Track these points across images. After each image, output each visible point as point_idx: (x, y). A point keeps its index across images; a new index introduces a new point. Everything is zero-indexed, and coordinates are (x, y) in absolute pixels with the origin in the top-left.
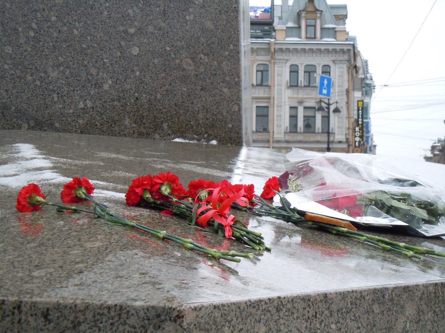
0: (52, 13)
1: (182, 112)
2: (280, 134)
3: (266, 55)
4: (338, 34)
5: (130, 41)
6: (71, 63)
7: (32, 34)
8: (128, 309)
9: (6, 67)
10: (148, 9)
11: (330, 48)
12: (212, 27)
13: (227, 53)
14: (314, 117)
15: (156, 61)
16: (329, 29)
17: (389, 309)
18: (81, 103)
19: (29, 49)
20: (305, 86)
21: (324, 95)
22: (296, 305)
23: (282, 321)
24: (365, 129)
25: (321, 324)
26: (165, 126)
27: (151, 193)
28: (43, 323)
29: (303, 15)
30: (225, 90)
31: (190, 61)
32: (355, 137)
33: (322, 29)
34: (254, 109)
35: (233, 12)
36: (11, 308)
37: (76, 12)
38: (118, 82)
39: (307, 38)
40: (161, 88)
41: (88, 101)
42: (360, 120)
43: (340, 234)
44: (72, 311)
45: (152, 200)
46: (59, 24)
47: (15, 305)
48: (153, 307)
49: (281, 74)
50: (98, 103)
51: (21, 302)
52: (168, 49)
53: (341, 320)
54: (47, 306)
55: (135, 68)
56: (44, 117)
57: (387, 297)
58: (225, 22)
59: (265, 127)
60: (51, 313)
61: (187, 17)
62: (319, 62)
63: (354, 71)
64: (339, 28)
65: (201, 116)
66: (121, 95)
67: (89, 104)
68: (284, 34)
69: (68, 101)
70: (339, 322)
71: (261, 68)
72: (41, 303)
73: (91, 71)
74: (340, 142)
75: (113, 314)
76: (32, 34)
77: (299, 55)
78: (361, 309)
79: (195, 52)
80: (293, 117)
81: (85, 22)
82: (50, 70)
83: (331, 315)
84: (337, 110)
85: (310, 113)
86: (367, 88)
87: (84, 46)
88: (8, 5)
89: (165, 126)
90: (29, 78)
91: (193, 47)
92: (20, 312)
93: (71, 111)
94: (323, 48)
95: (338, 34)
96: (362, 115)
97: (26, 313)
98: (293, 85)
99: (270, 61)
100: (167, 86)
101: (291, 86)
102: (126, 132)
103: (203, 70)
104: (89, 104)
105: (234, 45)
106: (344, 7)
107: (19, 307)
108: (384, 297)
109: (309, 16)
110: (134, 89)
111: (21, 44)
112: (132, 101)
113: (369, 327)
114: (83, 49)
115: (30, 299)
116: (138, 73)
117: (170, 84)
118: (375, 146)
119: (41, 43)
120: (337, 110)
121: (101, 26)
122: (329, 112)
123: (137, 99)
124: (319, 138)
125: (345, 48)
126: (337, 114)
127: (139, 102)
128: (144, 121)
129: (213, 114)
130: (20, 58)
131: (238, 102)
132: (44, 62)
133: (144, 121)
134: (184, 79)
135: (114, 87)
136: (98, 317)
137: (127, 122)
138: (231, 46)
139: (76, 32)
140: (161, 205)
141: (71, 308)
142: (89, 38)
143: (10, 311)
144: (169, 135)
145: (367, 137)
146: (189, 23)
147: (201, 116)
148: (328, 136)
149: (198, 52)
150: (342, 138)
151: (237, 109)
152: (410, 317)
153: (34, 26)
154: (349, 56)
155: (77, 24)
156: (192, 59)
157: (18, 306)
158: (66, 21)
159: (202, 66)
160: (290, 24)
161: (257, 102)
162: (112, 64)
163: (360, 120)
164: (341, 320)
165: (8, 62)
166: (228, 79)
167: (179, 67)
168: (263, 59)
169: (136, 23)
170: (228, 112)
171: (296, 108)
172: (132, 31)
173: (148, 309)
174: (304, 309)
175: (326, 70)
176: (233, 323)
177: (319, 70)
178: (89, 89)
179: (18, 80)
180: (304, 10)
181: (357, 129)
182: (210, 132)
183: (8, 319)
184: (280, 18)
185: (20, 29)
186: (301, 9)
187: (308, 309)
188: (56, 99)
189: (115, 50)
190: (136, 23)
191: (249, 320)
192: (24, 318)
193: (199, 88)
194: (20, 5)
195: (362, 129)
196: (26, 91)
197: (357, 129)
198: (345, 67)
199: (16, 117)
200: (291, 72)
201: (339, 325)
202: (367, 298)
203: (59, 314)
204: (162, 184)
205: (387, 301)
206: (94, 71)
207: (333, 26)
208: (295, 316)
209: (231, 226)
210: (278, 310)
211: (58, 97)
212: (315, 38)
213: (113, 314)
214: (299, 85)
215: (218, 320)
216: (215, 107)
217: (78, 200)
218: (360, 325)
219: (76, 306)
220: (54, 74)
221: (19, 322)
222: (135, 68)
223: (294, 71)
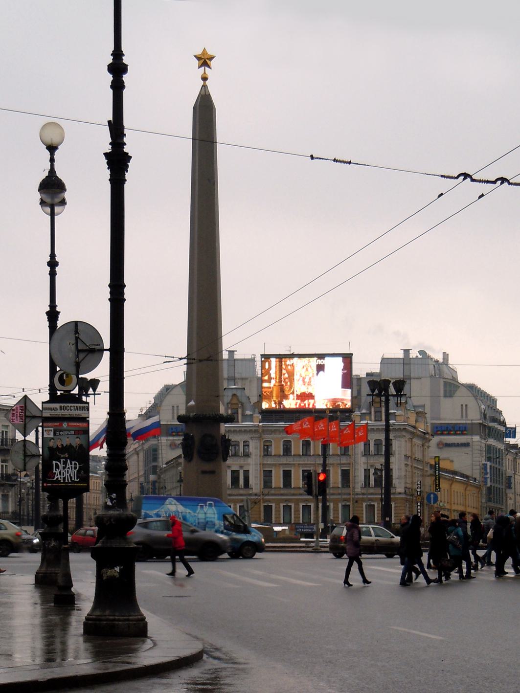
4: (397, 417)
39: (375, 420)
74: (400, 493)
77: (381, 433)
80: (367, 477)
98: (367, 453)
150: (402, 490)
160: (364, 411)
175: (246, 444)
200: (374, 444)
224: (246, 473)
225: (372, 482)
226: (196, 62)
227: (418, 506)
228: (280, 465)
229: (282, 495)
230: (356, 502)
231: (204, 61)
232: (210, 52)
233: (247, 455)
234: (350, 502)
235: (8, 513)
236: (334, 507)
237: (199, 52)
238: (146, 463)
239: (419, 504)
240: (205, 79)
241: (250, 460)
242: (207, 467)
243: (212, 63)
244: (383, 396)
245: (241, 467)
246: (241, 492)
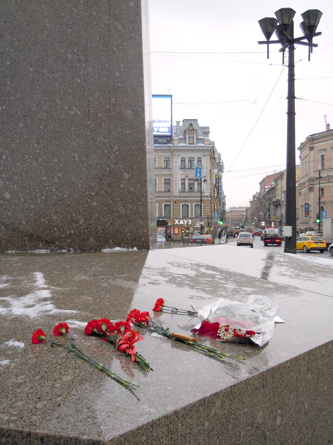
0: (53, 187)
1: (119, 233)
2: (177, 193)
3: (169, 153)
4: (205, 141)
5: (92, 199)
6: (63, 212)
7: (44, 198)
8: (80, 440)
9: (31, 215)
10: (101, 182)
11: (201, 148)
12: (133, 190)
13: (141, 203)
14: (194, 184)
15: (106, 208)
16: (200, 139)
17: (208, 407)
18: (69, 231)
19: (42, 206)
20: (189, 168)
21: (198, 176)
22: (161, 421)
23: (154, 431)
24: (219, 189)
25: (174, 425)
26: (111, 241)
27: (97, 329)
28: (41, 443)
29: (187, 132)
30: (141, 222)
31: (123, 208)
32: (215, 193)
33: (197, 139)
34: (163, 180)
35: (144, 182)
36: (26, 434)
37: (65, 185)
38: (87, 220)
40: (108, 222)
41: (72, 230)
42: (217, 184)
43: (189, 344)
44: (54, 438)
45: (97, 332)
46: (57, 192)
47: (27, 433)
48: (91, 440)
49: (176, 162)
50: (77, 231)
51: (30, 432)
52: (112, 202)
53: (183, 420)
54: (42, 435)
55: (95, 213)
56: (50, 240)
57: (206, 401)
58: (140, 187)
59: (169, 189)
60: (44, 438)
61: (121, 186)
62: (196, 156)
63: (214, 160)
64: (206, 138)
65: (128, 235)
66: (88, 226)
67: (72, 232)
68: (177, 141)
69: (62, 230)
70: (182, 422)
71: (166, 159)
72: (39, 433)
73: (73, 215)
74: (207, 197)
75: (73, 441)
76: (44, 198)
78: (194, 411)
79: (125, 203)
80: (183, 184)
81: (70, 191)
82: (53, 215)
83: (179, 419)
84: (205, 181)
85: (192, 182)
86: (220, 168)
87: (69, 202)
88: (32, 184)
89: (111, 241)
90: (43, 220)
91: (124, 201)
92: (30, 437)
93: (64, 236)
94: (197, 148)
95: (205, 142)
96: (218, 182)
97: (33, 438)
98: (183, 168)
99: (171, 156)
100: (111, 221)
101: (181, 168)
102: (91, 245)
103: (129, 212)
104: (72, 232)
105: (144, 199)
106: (208, 128)
107: (30, 435)
108: (205, 402)
109: (190, 132)
110: (95, 223)
111: (38, 203)
112: (94, 229)
113: (198, 418)
114: (69, 204)
115: (34, 431)
116: (96, 215)
117: (113, 220)
118: (225, 196)
119: (48, 202)
120: (205, 181)
121: (78, 192)
122: (201, 182)
123: (96, 228)
124: (196, 195)
125: (209, 149)
126: (205, 182)
127: (97, 230)
128: (100, 239)
129: (134, 234)
130: (38, 210)
131: (147, 227)
132: (50, 212)
133: (100, 239)
134: (120, 217)
135: (85, 223)
136: (66, 442)
137: (91, 240)
138: (143, 199)
139: (65, 196)
140: (102, 336)
141: (53, 437)
142: (72, 198)
143: (25, 436)
144: (113, 245)
145: (221, 193)
146: (121, 188)
147: (128, 235)
148: (201, 194)
149: (126, 203)
150: (208, 194)
151: (146, 231)
152: (218, 407)
153: (45, 194)
154: (211, 152)
155: (66, 192)
156: (124, 206)
157: (29, 434)
158: (60, 190)
159: (128, 210)
160: (181, 137)
161: (164, 177)
162: (83, 211)
163: (217, 184)
164: (183, 420)
165: (33, 212)
166: (142, 216)
167: (117, 211)
168: (167, 154)
169: (95, 190)
170: (142, 233)
171: (185, 179)
172: (93, 194)
173: (89, 441)
174: (165, 421)
175: (199, 161)
176: (130, 440)
177: (196, 160)
178: (72, 224)
179: (37, 221)
180: (187, 130)
181: (216, 190)
182: (133, 243)
183: (24, 440)
184: (176, 134)
185: (38, 196)
186: (187, 129)
187: (167, 421)
188: (56, 230)
189: (85, 204)
190: (95, 190)
191: (138, 436)
192: (32, 440)
193: (127, 221)
194: (38, 184)
195: (218, 189)
196: (41, 227)
197: (216, 190)
198: (209, 158)
199: (37, 240)
201: (182, 423)
202: (196, 405)
203: (48, 440)
204: (102, 324)
205: (206, 403)
206: (74, 215)
207: (203, 137)
208: (161, 426)
209: (134, 355)
210: (152, 426)
211: (57, 229)
212: (193, 143)
213: (73, 441)
214: (186, 168)
215: (122, 441)
216: (135, 230)
217: (61, 334)
218: (193, 419)
219: (56, 436)
220: (55, 218)
221: (30, 441)
222: (95, 213)
223: (183, 161)
225: (187, 187)
227: (215, 206)
228: (162, 175)
230: (176, 202)
234: (171, 202)
236: (159, 206)
239: (216, 204)
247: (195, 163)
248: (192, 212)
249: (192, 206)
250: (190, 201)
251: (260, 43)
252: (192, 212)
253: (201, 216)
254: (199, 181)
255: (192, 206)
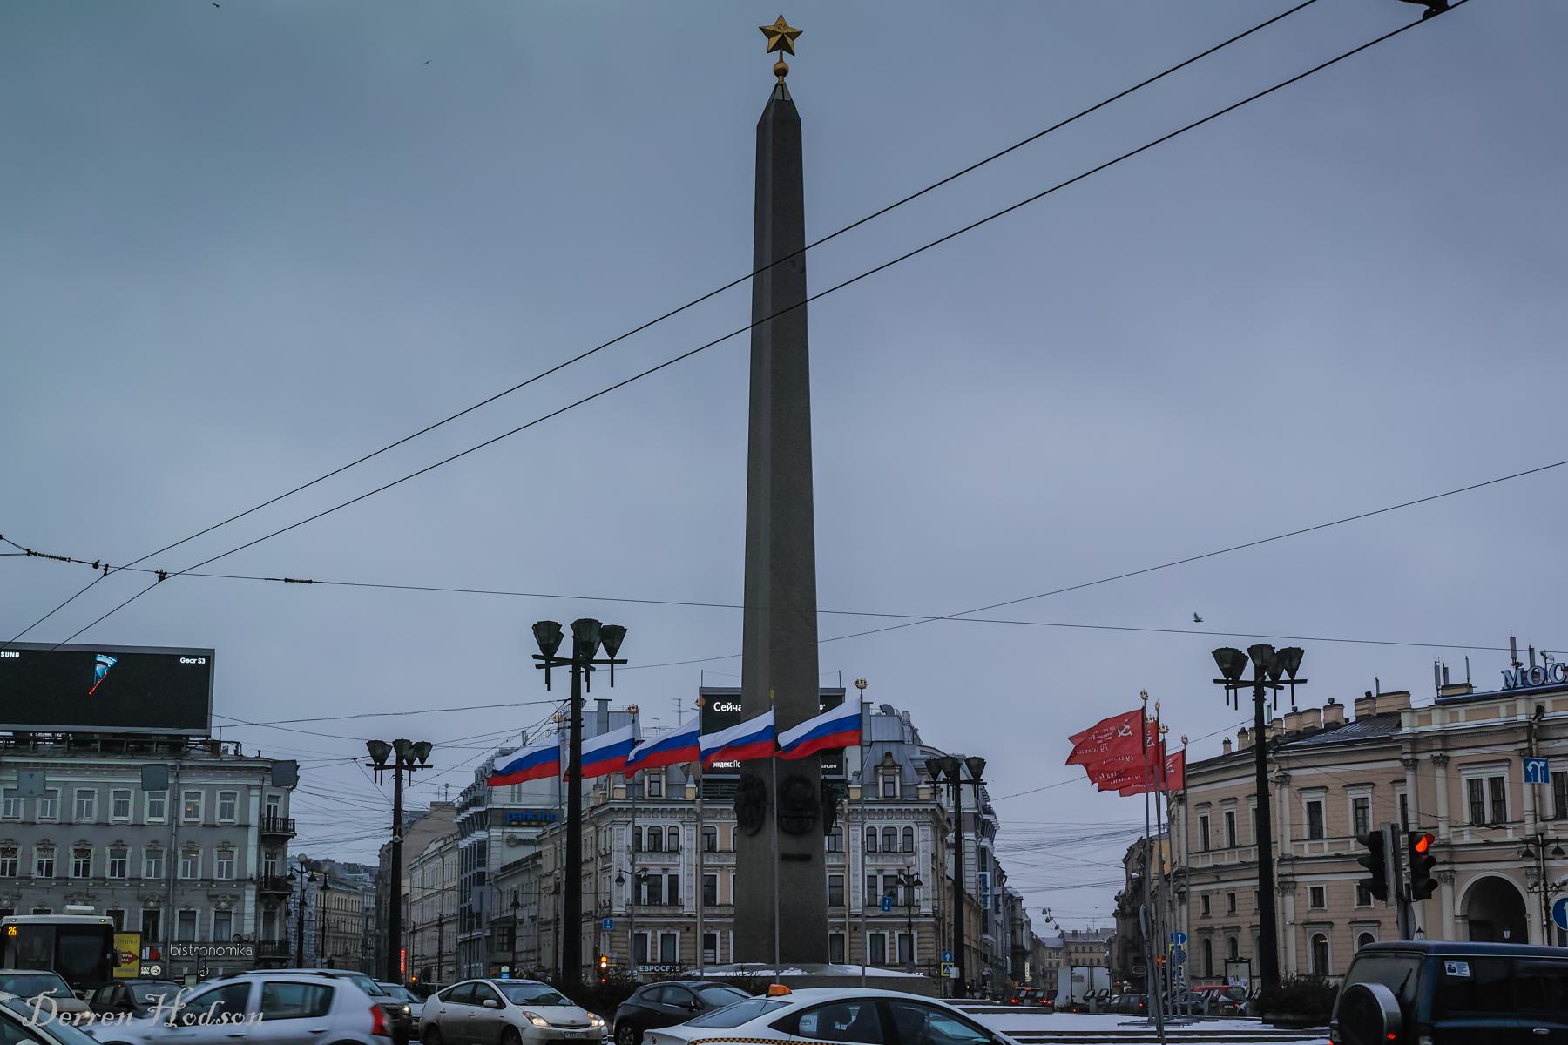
62: (900, 823)
85: (891, 883)
124: (901, 912)
150: (929, 910)
175: (908, 834)
224: (674, 881)
226: (764, 42)
229: (664, 916)
231: (782, 40)
232: (793, 24)
233: (676, 851)
235: (273, 943)
237: (770, 23)
238: (464, 867)
240: (781, 72)
241: (679, 859)
242: (793, 845)
243: (797, 44)
244: (562, 662)
245: (665, 870)
246: (665, 911)
247: (900, 838)
248: (893, 950)
249: (892, 937)
250: (651, 925)
251: (1216, 681)
252: (893, 950)
253: (911, 958)
254: (912, 883)
255: (892, 937)
